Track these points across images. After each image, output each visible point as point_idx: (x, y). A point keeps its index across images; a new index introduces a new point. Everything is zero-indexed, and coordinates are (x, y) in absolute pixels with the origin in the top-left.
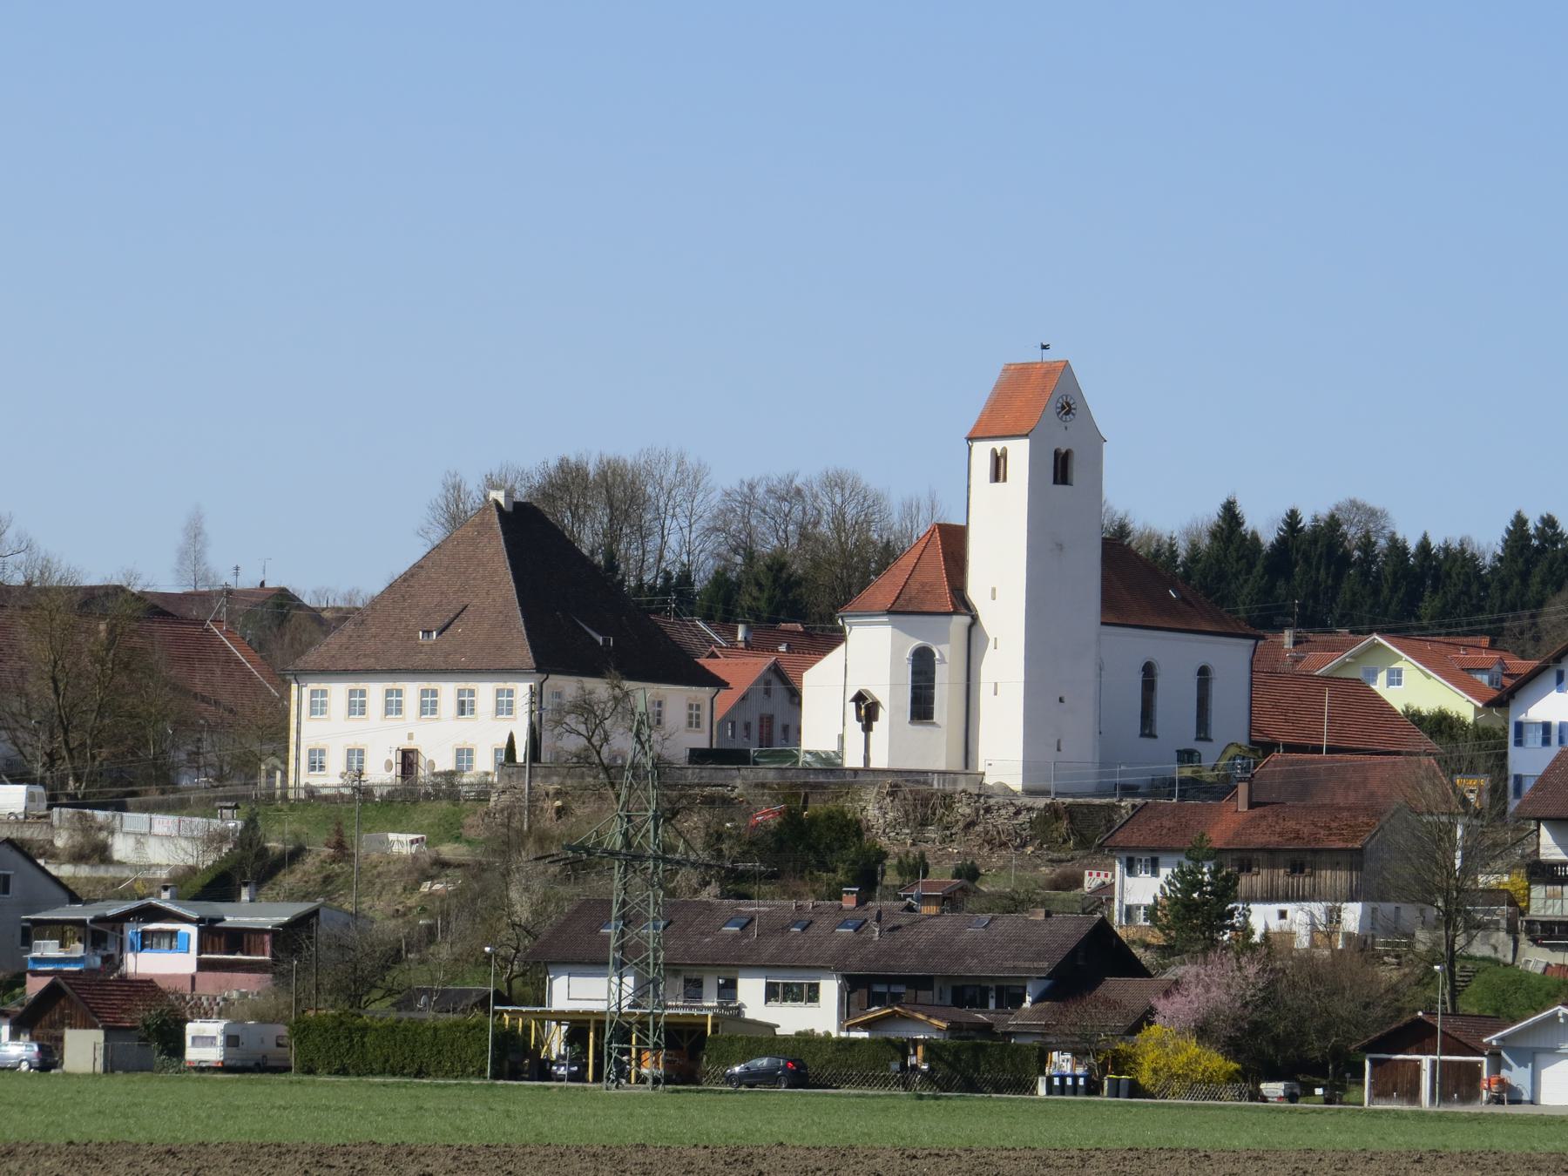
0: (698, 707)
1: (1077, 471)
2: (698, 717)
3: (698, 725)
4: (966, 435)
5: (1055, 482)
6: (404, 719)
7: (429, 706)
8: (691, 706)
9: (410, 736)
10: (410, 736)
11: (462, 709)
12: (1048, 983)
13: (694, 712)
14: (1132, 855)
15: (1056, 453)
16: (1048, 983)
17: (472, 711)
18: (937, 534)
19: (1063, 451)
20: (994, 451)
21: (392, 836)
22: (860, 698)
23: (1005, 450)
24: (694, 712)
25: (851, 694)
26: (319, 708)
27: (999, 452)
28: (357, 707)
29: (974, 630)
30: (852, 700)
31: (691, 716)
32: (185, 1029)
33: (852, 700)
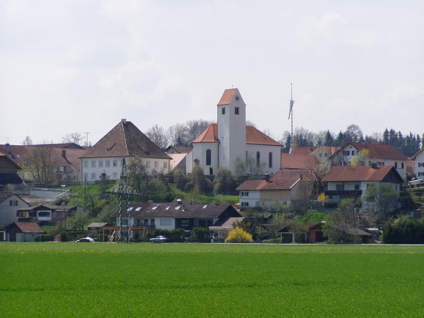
0: (166, 163)
1: (240, 111)
2: (166, 165)
3: (166, 167)
4: (217, 104)
5: (235, 114)
6: (117, 167)
7: (108, 165)
8: (164, 163)
9: (104, 171)
10: (104, 171)
11: (114, 165)
12: (218, 219)
13: (101, 163)
14: (243, 191)
15: (235, 108)
16: (218, 219)
17: (116, 165)
18: (212, 126)
19: (237, 107)
20: (222, 108)
21: (236, 189)
22: (196, 160)
23: (225, 107)
24: (108, 163)
25: (194, 159)
26: (86, 166)
27: (223, 108)
28: (93, 165)
29: (219, 145)
30: (194, 161)
31: (164, 165)
32: (229, 218)
33: (194, 161)
